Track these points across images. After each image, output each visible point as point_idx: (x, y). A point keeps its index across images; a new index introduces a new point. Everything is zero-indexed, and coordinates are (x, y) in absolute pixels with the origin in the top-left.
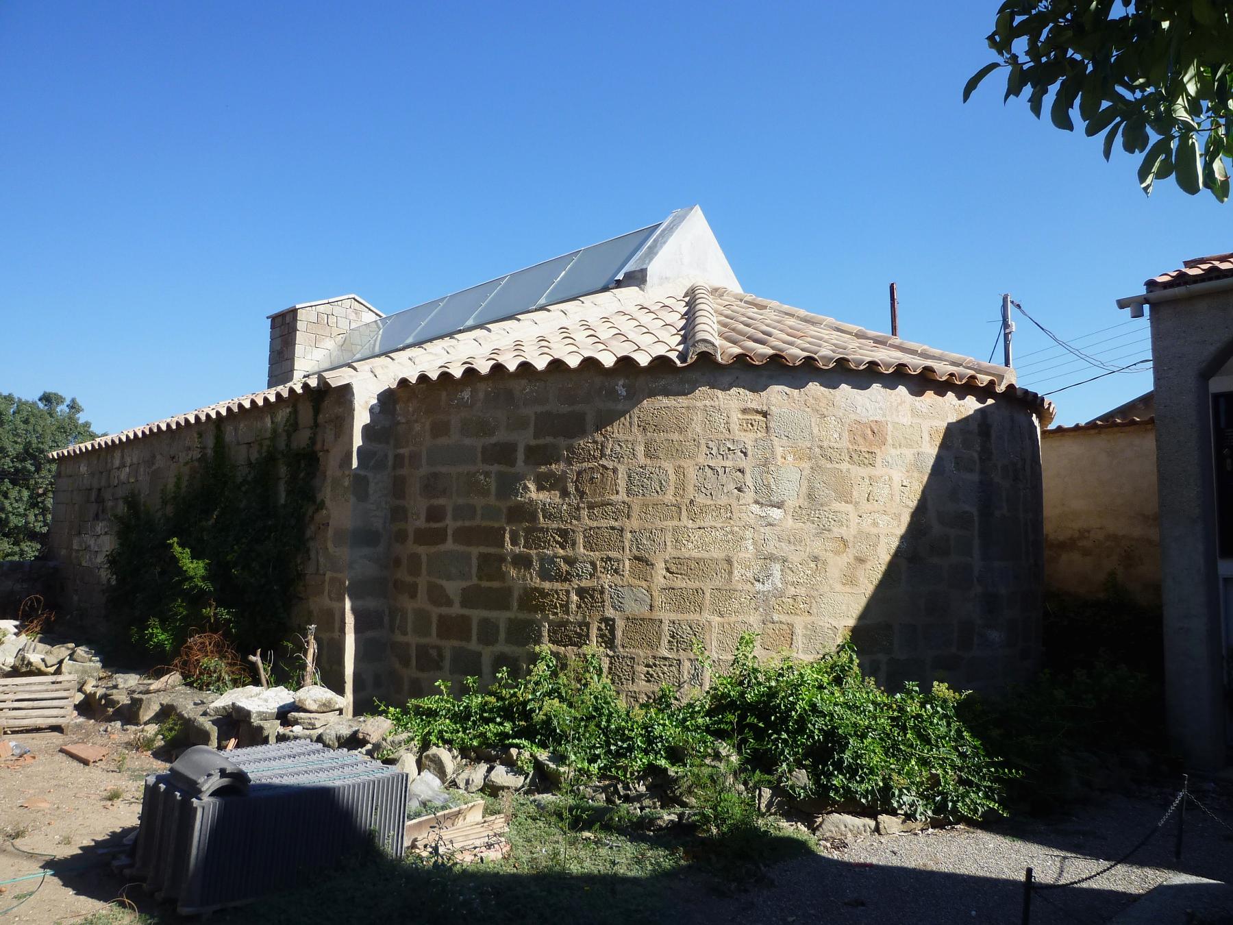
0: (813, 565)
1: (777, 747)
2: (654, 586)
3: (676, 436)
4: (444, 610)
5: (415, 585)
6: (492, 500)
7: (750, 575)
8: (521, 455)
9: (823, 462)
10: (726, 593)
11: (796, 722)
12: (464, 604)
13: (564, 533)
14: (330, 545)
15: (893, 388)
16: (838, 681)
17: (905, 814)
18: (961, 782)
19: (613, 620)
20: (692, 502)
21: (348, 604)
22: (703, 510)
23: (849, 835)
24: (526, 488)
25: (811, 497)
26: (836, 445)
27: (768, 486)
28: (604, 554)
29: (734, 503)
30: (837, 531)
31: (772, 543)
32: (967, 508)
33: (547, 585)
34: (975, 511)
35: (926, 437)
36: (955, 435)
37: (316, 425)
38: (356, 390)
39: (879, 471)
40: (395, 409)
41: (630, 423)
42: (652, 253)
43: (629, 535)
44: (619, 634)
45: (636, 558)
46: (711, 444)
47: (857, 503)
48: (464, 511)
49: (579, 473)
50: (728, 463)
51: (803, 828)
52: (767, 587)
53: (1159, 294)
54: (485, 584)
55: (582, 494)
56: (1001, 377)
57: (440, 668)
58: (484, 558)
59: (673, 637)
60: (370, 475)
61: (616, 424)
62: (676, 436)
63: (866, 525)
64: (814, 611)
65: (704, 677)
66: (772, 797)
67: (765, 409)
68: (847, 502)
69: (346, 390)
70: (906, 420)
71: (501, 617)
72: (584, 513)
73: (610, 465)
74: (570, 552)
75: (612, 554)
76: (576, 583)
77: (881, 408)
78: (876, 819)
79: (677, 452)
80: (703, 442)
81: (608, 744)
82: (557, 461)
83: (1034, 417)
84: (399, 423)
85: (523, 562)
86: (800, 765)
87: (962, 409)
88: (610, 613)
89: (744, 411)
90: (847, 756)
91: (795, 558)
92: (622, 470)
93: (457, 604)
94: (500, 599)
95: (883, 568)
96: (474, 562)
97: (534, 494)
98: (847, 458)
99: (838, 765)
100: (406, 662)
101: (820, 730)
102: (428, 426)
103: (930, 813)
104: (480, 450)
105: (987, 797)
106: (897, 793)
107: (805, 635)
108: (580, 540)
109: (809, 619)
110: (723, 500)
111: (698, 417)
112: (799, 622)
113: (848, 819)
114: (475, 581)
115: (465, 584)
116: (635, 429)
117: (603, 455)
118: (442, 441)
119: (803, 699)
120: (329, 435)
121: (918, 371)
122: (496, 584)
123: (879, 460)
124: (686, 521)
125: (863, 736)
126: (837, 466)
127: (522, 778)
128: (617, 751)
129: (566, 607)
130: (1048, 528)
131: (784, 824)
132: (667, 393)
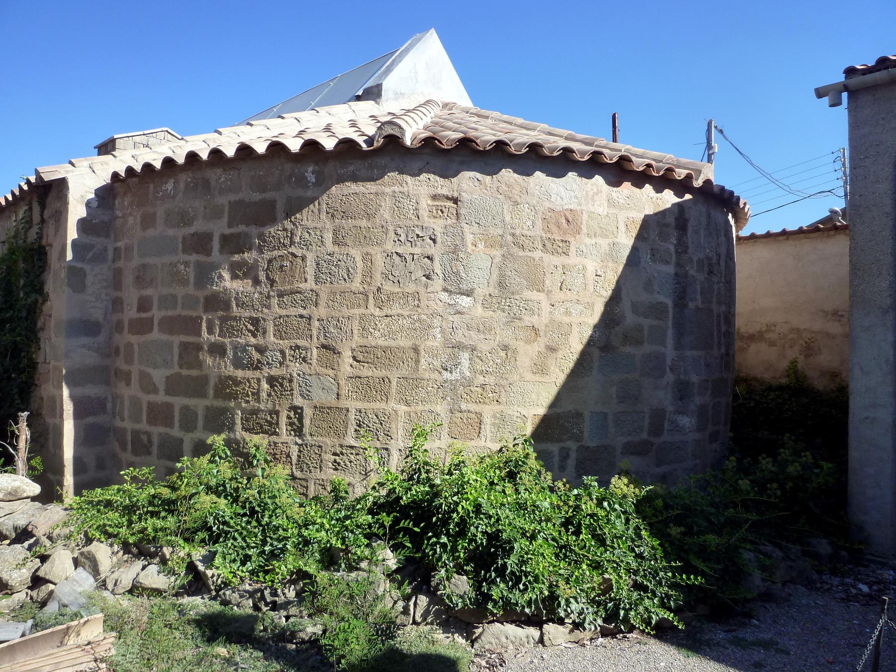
0: (503, 354)
1: (435, 553)
2: (340, 375)
3: (364, 223)
4: (152, 398)
5: (129, 374)
6: (191, 290)
7: (437, 364)
8: (216, 244)
9: (515, 250)
10: (413, 382)
11: (457, 525)
12: (168, 392)
13: (255, 322)
14: (53, 335)
15: (590, 177)
16: (512, 476)
17: (574, 622)
18: (637, 586)
19: (301, 408)
20: (379, 289)
21: (66, 392)
22: (391, 297)
23: (511, 647)
24: (220, 277)
25: (501, 285)
26: (528, 233)
27: (457, 274)
28: (292, 342)
29: (422, 290)
30: (528, 320)
31: (460, 332)
32: (662, 298)
33: (240, 374)
34: (669, 302)
35: (622, 228)
36: (651, 227)
37: (43, 221)
38: (71, 185)
39: (573, 259)
40: (114, 204)
41: (319, 210)
42: (389, 70)
43: (317, 324)
44: (307, 422)
45: (324, 347)
46: (399, 231)
47: (549, 292)
48: (169, 301)
49: (270, 261)
50: (417, 251)
51: (460, 640)
52: (455, 376)
53: (856, 80)
54: (185, 372)
55: (272, 282)
56: (699, 172)
57: (149, 453)
58: (184, 346)
59: (359, 426)
60: (87, 267)
61: (305, 211)
62: (364, 223)
63: (559, 316)
64: (503, 399)
65: (373, 474)
66: (428, 606)
67: (456, 195)
68: (539, 291)
69: (62, 184)
70: (602, 209)
71: (199, 405)
72: (275, 301)
73: (299, 252)
74: (260, 341)
75: (300, 343)
76: (266, 371)
77: (576, 197)
78: (541, 629)
79: (365, 238)
80: (391, 228)
81: (264, 542)
82: (250, 249)
83: (730, 217)
84: (117, 217)
85: (218, 350)
86: (460, 570)
87: (659, 202)
88: (298, 401)
89: (435, 197)
90: (511, 562)
91: (484, 347)
92: (310, 257)
93: (162, 392)
94: (197, 387)
95: (575, 357)
96: (176, 351)
97: (228, 283)
98: (540, 247)
99: (501, 571)
100: (124, 448)
101: (484, 533)
102: (139, 220)
103: (600, 621)
104: (180, 240)
105: (663, 605)
106: (563, 603)
107: (493, 424)
108: (271, 329)
109: (498, 408)
110: (411, 288)
111: (387, 204)
112: (488, 412)
113: (511, 629)
114: (176, 369)
115: (168, 372)
116: (323, 216)
117: (292, 243)
118: (151, 232)
119: (467, 499)
120: (50, 230)
121: (615, 160)
122: (194, 373)
123: (573, 249)
124: (372, 309)
125: (533, 538)
126: (529, 254)
127: (173, 579)
128: (272, 552)
129: (257, 395)
130: (741, 323)
131: (440, 635)
132: (355, 179)
